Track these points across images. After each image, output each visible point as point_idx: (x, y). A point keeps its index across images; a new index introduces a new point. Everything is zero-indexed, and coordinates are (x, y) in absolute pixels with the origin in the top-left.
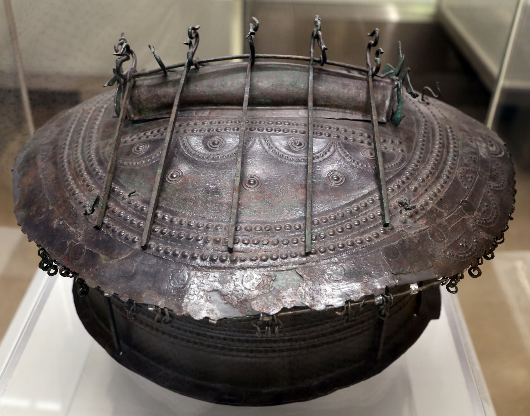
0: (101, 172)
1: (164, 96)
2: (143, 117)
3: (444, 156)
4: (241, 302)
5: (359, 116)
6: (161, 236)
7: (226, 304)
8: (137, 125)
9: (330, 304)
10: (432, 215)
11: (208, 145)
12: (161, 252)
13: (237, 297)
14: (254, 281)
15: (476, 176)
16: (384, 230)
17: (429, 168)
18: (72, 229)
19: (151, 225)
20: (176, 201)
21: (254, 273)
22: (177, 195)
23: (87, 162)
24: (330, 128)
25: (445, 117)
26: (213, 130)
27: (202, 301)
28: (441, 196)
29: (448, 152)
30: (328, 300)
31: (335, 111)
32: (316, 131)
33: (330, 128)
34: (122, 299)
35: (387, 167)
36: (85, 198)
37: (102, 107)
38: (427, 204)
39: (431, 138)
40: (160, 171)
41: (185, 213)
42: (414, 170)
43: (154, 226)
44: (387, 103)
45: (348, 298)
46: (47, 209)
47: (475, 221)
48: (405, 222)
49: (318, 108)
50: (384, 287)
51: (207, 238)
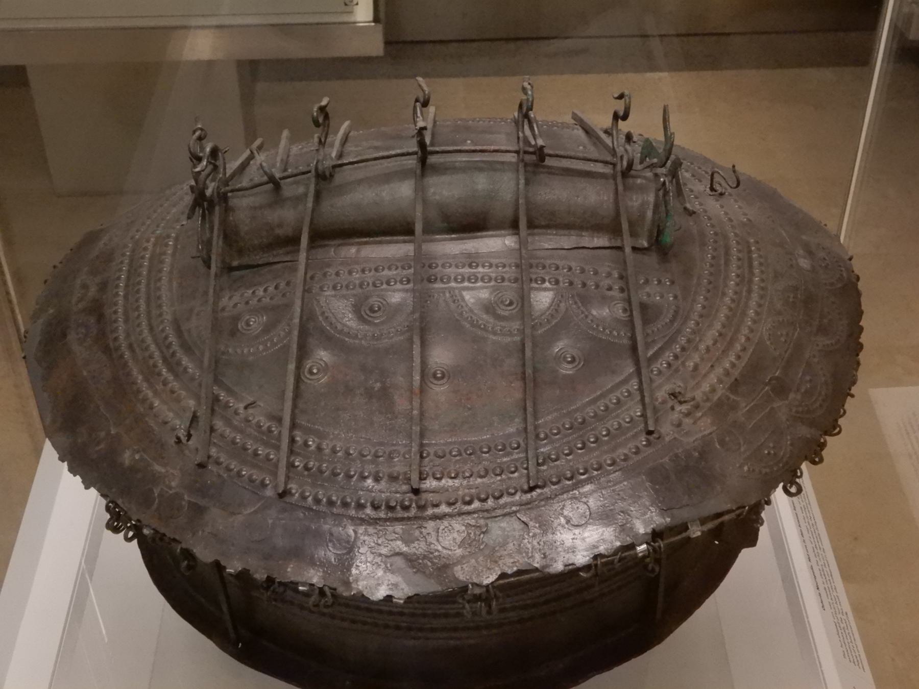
0: (191, 368)
1: (280, 226)
2: (246, 261)
3: (744, 300)
4: (439, 569)
5: (602, 241)
6: (306, 473)
7: (415, 573)
8: (237, 274)
9: (570, 562)
10: (721, 409)
11: (363, 313)
12: (310, 499)
13: (432, 562)
14: (455, 535)
15: (795, 329)
16: (648, 440)
17: (718, 326)
18: (158, 468)
19: (288, 458)
20: (322, 414)
21: (453, 522)
22: (323, 404)
23: (165, 350)
24: (557, 268)
25: (749, 220)
26: (368, 284)
27: (380, 573)
28: (736, 373)
29: (750, 291)
30: (567, 556)
31: (565, 235)
32: (534, 277)
33: (557, 268)
34: (257, 576)
35: (649, 331)
36: (171, 415)
37: (168, 236)
38: (713, 390)
39: (722, 268)
40: (292, 367)
41: (339, 434)
42: (694, 332)
43: (292, 458)
44: (649, 214)
45: (596, 551)
46: (108, 433)
47: (791, 410)
48: (679, 425)
49: (536, 231)
50: (649, 530)
51: (377, 472)
